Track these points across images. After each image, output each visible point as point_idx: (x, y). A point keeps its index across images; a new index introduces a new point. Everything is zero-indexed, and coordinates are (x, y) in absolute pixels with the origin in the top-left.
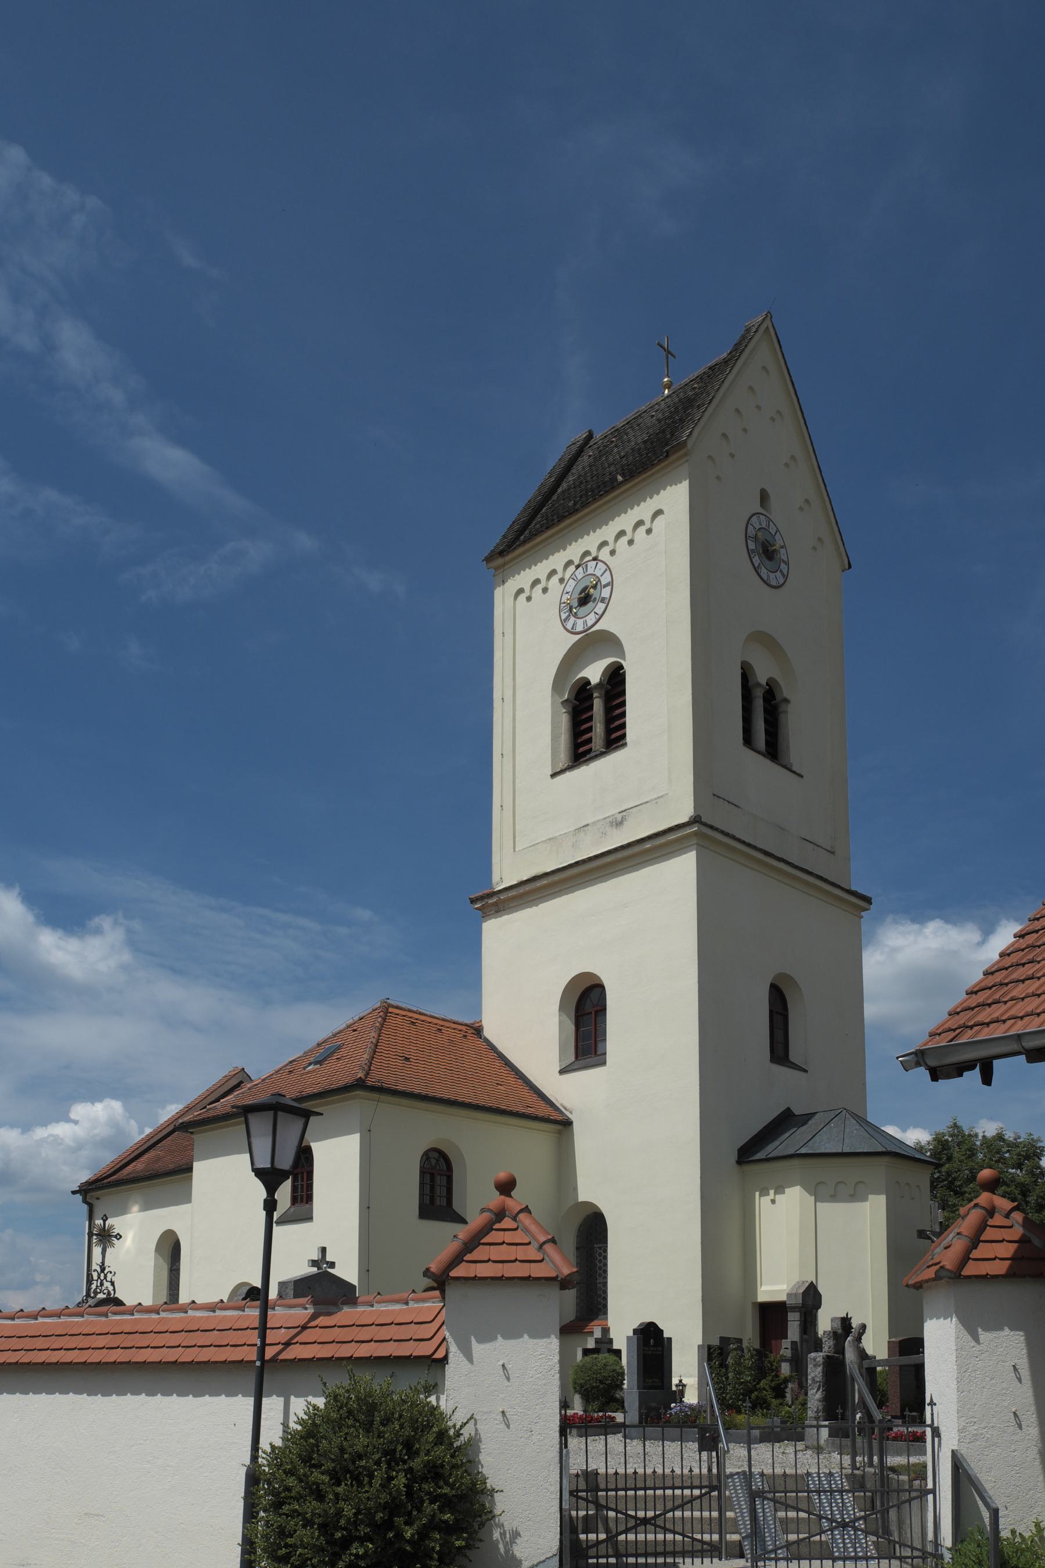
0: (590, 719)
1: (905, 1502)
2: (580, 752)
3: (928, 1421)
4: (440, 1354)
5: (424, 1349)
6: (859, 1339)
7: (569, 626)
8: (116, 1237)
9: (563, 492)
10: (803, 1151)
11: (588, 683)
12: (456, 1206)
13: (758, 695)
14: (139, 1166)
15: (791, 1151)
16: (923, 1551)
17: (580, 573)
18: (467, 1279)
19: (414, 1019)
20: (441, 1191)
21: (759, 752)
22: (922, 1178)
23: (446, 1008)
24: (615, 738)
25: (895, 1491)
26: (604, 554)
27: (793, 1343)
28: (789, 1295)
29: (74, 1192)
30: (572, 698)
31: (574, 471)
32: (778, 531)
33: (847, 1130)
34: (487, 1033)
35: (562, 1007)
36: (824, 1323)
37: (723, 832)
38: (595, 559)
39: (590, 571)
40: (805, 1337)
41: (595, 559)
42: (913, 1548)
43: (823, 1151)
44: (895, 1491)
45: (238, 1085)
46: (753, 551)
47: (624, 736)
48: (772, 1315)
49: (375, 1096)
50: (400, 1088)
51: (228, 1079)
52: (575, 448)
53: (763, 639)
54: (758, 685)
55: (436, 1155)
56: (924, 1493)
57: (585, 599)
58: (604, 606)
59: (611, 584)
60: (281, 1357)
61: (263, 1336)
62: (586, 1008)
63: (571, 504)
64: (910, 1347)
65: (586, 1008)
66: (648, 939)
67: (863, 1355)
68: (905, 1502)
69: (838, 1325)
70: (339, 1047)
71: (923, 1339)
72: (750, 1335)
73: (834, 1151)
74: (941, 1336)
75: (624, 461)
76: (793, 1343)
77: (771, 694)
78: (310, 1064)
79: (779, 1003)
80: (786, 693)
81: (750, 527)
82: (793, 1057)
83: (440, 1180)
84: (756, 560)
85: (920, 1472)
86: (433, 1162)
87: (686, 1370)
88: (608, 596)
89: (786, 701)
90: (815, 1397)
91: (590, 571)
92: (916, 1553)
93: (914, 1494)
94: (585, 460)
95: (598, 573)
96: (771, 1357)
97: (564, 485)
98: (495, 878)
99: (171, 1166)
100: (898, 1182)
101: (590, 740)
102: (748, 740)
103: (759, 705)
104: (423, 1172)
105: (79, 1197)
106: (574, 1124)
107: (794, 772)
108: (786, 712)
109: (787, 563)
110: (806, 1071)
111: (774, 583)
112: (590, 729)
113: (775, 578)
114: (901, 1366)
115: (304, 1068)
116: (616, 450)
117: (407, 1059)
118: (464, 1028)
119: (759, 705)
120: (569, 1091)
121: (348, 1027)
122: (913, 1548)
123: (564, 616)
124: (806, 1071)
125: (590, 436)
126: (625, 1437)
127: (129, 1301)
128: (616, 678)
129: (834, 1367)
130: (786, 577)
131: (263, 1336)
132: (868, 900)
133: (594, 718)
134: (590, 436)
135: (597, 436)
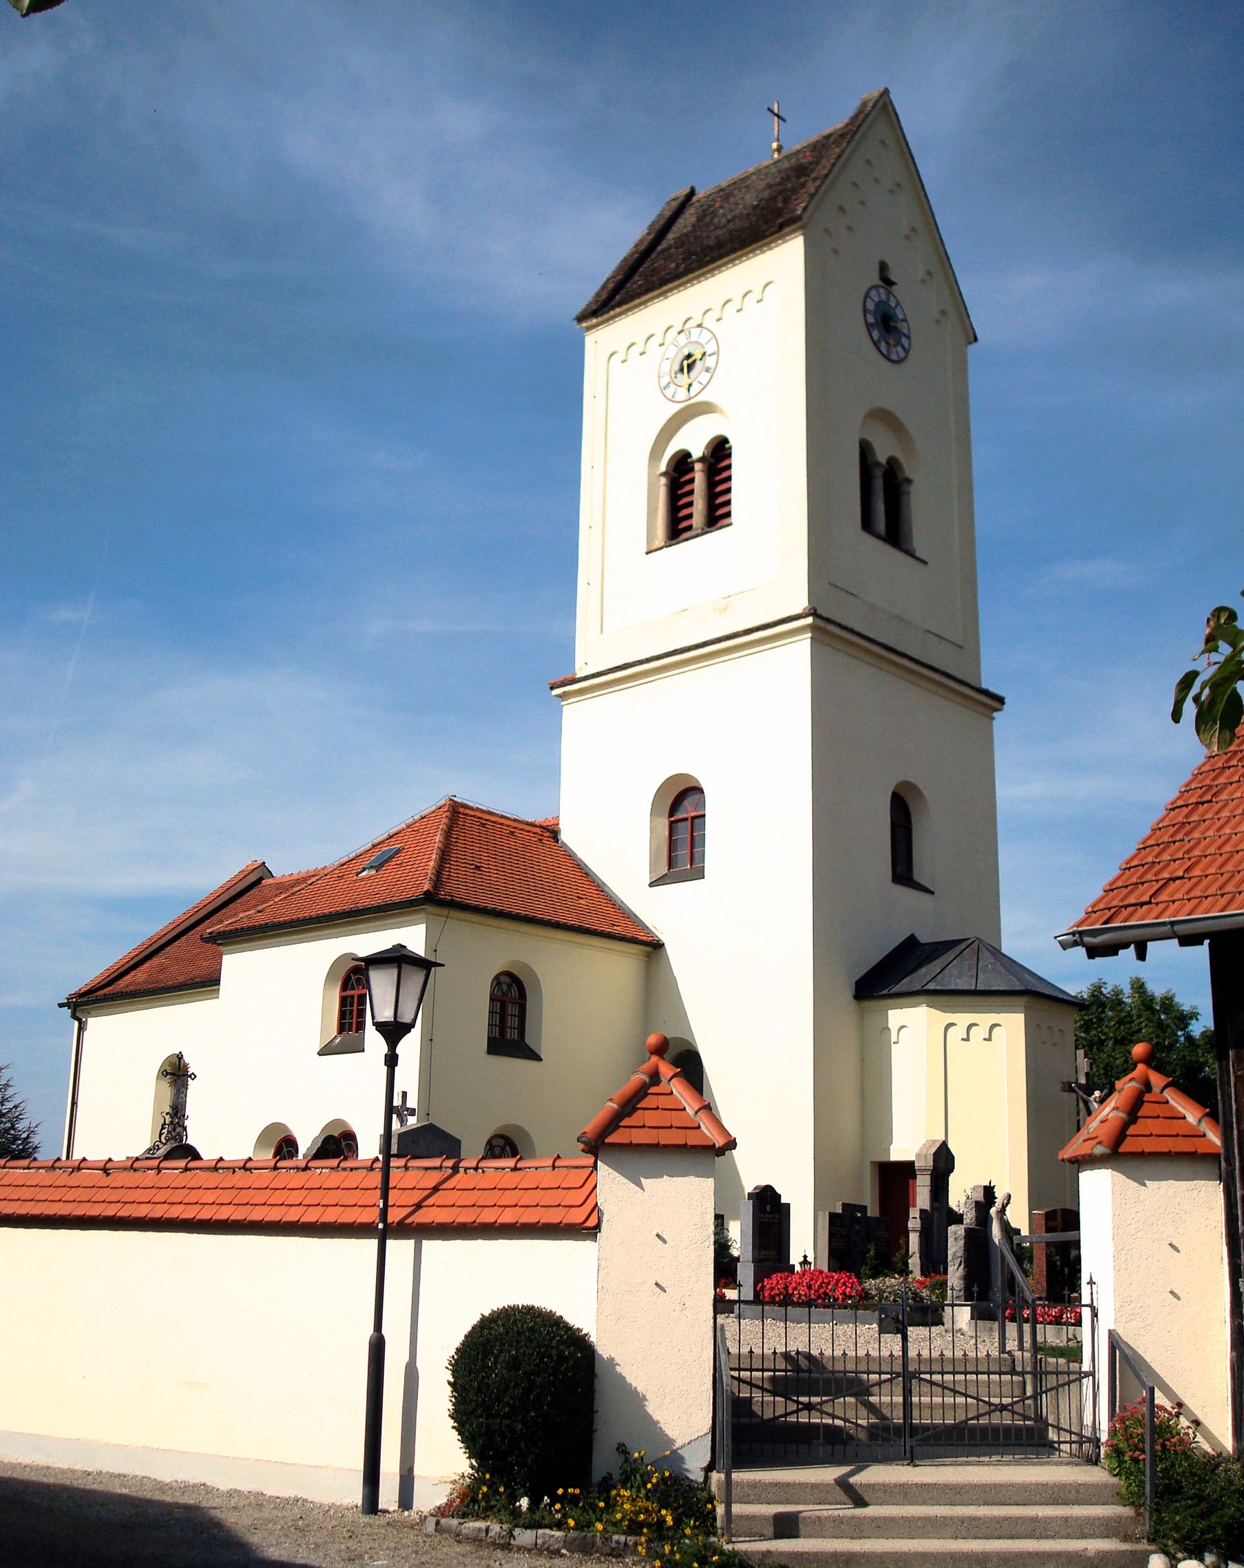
0: (691, 492)
1: (1063, 1385)
2: (677, 530)
3: (1086, 1299)
4: (592, 1222)
5: (576, 1216)
6: (1002, 1211)
7: (669, 395)
8: (167, 1074)
9: (664, 250)
10: (931, 986)
11: (688, 455)
12: (529, 1040)
13: (878, 473)
14: (139, 976)
15: (917, 987)
16: (1080, 1435)
17: (682, 339)
18: (620, 1145)
19: (486, 821)
20: (512, 1022)
21: (878, 537)
22: (1069, 1023)
23: (527, 810)
24: (717, 516)
25: (1052, 1373)
26: (709, 321)
27: (922, 1211)
28: (918, 1155)
29: (61, 1005)
30: (671, 470)
31: (674, 229)
32: (898, 303)
33: (980, 964)
34: (564, 837)
35: (654, 811)
36: (960, 1193)
37: (840, 626)
38: (699, 326)
39: (694, 337)
40: (936, 1205)
41: (699, 326)
42: (1071, 1433)
43: (953, 987)
44: (1052, 1373)
45: (258, 882)
46: (872, 325)
47: (728, 515)
48: (895, 1177)
49: (445, 911)
50: (472, 902)
51: (245, 874)
52: (675, 204)
53: (883, 416)
54: (878, 464)
55: (507, 979)
56: (1082, 1375)
57: (689, 364)
58: (709, 375)
59: (717, 353)
60: (409, 1221)
61: (385, 1197)
62: (681, 806)
63: (673, 265)
64: (1062, 1220)
65: (681, 806)
66: (757, 738)
67: (1005, 1226)
68: (1063, 1385)
69: (980, 1196)
70: (399, 851)
71: (1078, 1214)
72: (869, 1199)
73: (966, 987)
74: (1098, 1190)
75: (731, 226)
76: (922, 1211)
77: (893, 466)
78: (364, 870)
79: (902, 810)
80: (908, 472)
81: (869, 302)
82: (918, 876)
83: (511, 1009)
84: (876, 334)
85: (1074, 1354)
86: (505, 987)
87: (804, 1241)
88: (713, 366)
89: (909, 481)
90: (955, 1276)
91: (694, 337)
92: (1074, 1438)
93: (1072, 1377)
94: (688, 219)
95: (702, 341)
96: (887, 1223)
97: (664, 245)
98: (579, 663)
99: (181, 979)
100: (1038, 1026)
101: (690, 516)
102: (867, 524)
103: (879, 484)
104: (493, 999)
105: (67, 1012)
106: (670, 948)
107: (937, 635)
108: (908, 493)
109: (908, 337)
110: (932, 893)
111: (894, 357)
112: (691, 504)
113: (898, 352)
114: (1048, 1244)
115: (358, 874)
116: (721, 211)
117: (478, 868)
118: (538, 830)
119: (879, 484)
120: (658, 909)
121: (408, 827)
122: (1071, 1433)
123: (664, 382)
124: (932, 893)
125: (692, 192)
126: (739, 1317)
127: (208, 1153)
128: (720, 450)
129: (977, 1239)
130: (907, 351)
131: (385, 1197)
132: (1001, 700)
133: (695, 492)
134: (692, 192)
135: (701, 193)
